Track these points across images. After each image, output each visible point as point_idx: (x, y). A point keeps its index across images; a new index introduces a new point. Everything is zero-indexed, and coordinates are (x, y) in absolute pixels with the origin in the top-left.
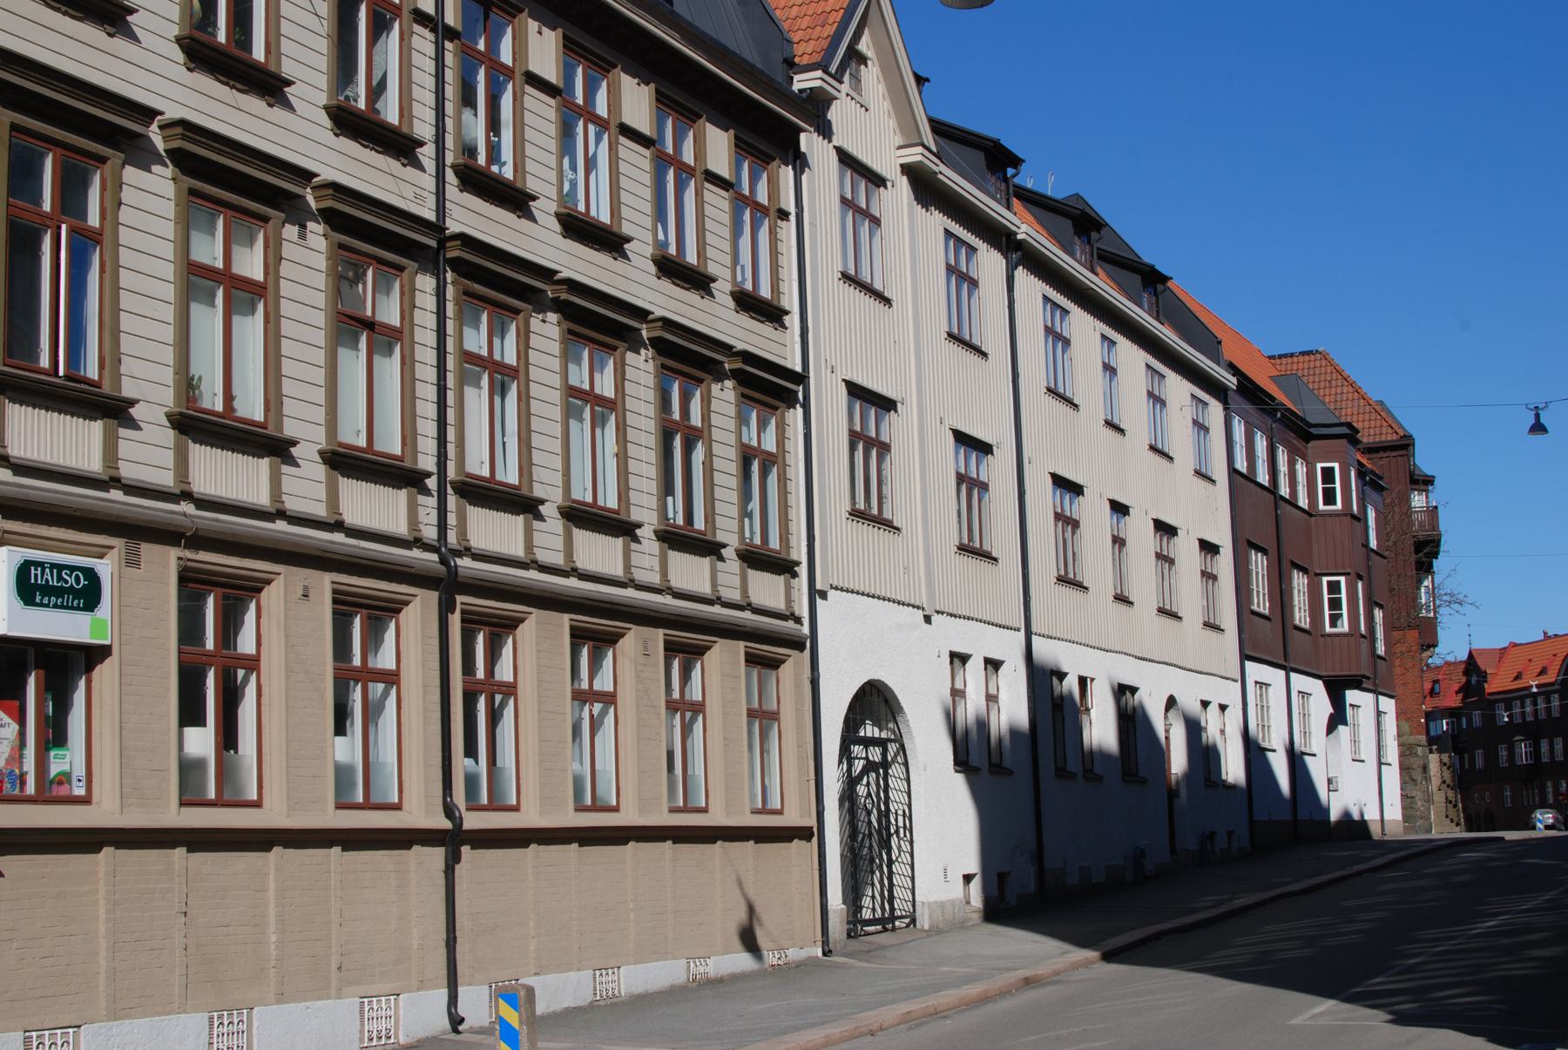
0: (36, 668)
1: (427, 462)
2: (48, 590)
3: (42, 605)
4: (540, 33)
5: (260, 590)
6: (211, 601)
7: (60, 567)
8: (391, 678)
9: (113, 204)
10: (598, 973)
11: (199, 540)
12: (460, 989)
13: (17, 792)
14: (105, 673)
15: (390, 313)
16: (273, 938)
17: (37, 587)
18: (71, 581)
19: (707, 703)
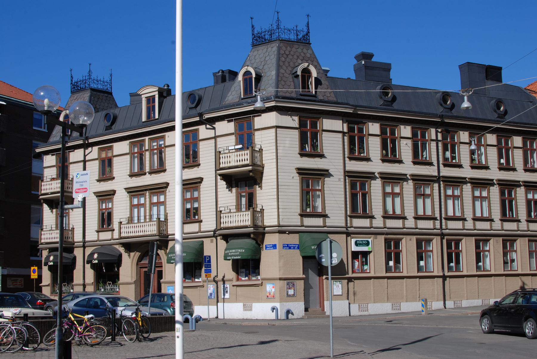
0: (360, 254)
1: (437, 215)
2: (360, 244)
3: (359, 246)
4: (464, 134)
5: (432, 240)
6: (508, 243)
7: (362, 241)
8: (432, 251)
9: (516, 193)
10: (483, 300)
11: (387, 234)
12: (446, 302)
13: (358, 272)
14: (372, 255)
15: (428, 191)
16: (405, 292)
17: (358, 244)
18: (364, 242)
19: (517, 250)
